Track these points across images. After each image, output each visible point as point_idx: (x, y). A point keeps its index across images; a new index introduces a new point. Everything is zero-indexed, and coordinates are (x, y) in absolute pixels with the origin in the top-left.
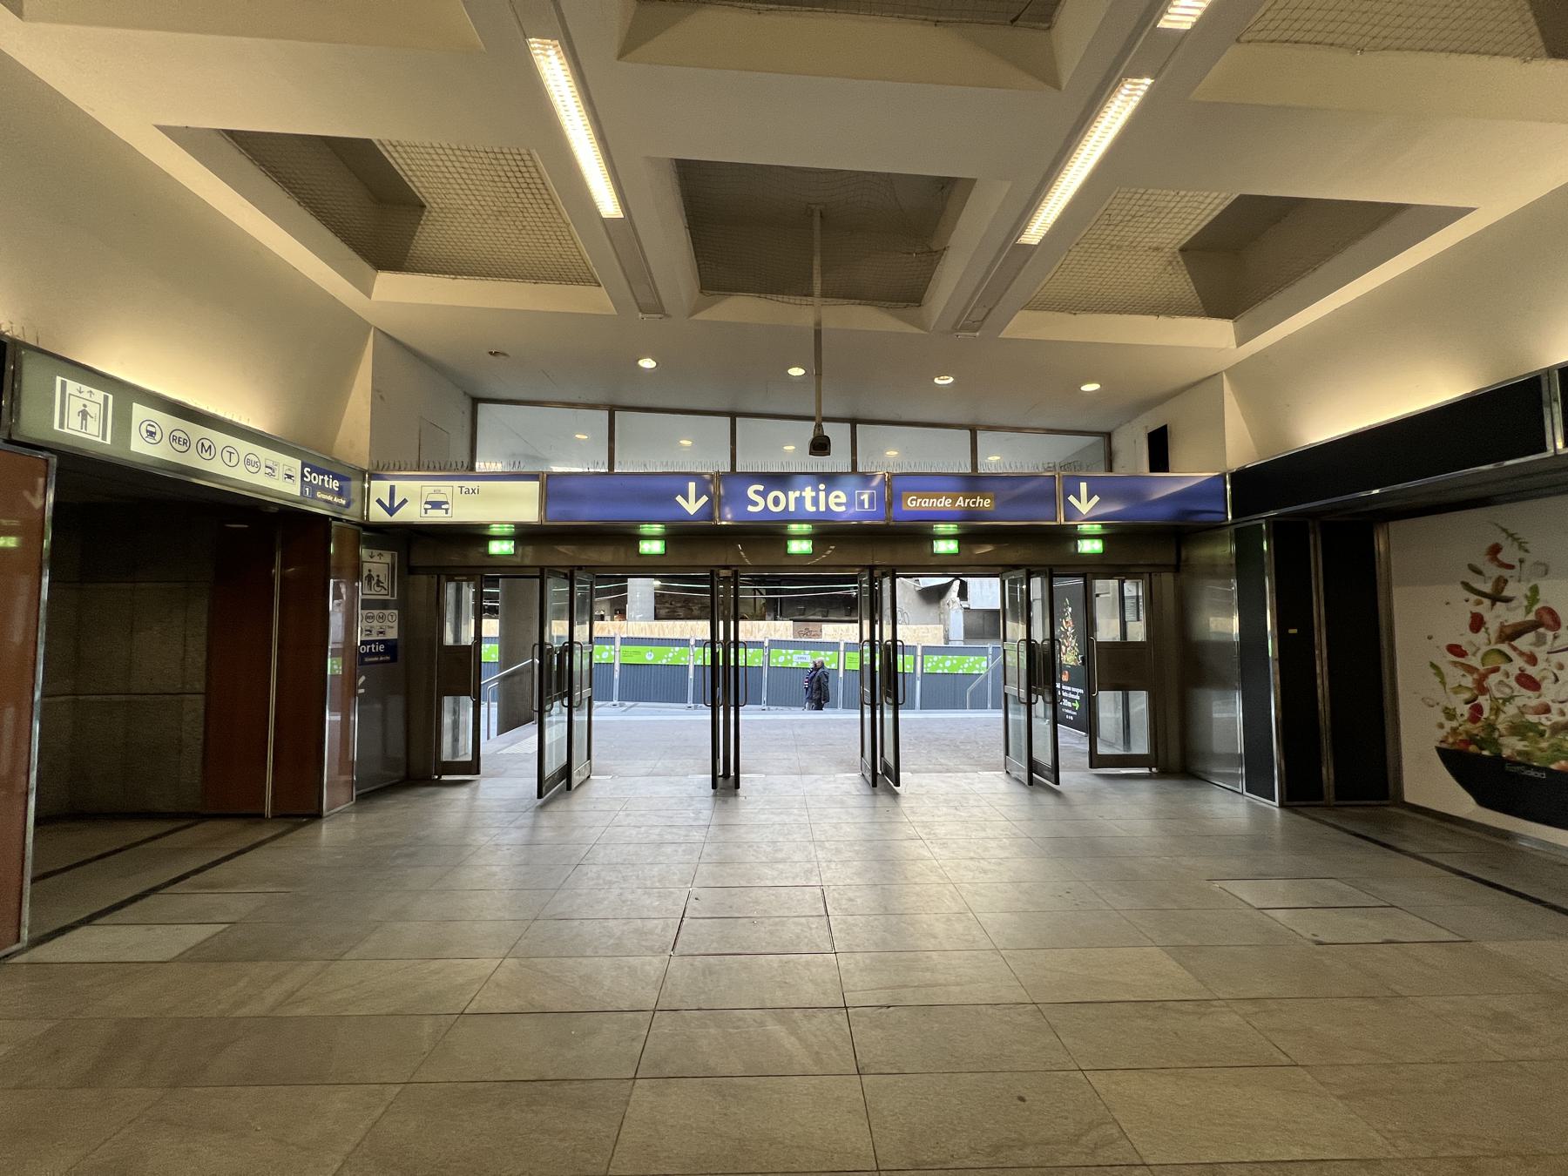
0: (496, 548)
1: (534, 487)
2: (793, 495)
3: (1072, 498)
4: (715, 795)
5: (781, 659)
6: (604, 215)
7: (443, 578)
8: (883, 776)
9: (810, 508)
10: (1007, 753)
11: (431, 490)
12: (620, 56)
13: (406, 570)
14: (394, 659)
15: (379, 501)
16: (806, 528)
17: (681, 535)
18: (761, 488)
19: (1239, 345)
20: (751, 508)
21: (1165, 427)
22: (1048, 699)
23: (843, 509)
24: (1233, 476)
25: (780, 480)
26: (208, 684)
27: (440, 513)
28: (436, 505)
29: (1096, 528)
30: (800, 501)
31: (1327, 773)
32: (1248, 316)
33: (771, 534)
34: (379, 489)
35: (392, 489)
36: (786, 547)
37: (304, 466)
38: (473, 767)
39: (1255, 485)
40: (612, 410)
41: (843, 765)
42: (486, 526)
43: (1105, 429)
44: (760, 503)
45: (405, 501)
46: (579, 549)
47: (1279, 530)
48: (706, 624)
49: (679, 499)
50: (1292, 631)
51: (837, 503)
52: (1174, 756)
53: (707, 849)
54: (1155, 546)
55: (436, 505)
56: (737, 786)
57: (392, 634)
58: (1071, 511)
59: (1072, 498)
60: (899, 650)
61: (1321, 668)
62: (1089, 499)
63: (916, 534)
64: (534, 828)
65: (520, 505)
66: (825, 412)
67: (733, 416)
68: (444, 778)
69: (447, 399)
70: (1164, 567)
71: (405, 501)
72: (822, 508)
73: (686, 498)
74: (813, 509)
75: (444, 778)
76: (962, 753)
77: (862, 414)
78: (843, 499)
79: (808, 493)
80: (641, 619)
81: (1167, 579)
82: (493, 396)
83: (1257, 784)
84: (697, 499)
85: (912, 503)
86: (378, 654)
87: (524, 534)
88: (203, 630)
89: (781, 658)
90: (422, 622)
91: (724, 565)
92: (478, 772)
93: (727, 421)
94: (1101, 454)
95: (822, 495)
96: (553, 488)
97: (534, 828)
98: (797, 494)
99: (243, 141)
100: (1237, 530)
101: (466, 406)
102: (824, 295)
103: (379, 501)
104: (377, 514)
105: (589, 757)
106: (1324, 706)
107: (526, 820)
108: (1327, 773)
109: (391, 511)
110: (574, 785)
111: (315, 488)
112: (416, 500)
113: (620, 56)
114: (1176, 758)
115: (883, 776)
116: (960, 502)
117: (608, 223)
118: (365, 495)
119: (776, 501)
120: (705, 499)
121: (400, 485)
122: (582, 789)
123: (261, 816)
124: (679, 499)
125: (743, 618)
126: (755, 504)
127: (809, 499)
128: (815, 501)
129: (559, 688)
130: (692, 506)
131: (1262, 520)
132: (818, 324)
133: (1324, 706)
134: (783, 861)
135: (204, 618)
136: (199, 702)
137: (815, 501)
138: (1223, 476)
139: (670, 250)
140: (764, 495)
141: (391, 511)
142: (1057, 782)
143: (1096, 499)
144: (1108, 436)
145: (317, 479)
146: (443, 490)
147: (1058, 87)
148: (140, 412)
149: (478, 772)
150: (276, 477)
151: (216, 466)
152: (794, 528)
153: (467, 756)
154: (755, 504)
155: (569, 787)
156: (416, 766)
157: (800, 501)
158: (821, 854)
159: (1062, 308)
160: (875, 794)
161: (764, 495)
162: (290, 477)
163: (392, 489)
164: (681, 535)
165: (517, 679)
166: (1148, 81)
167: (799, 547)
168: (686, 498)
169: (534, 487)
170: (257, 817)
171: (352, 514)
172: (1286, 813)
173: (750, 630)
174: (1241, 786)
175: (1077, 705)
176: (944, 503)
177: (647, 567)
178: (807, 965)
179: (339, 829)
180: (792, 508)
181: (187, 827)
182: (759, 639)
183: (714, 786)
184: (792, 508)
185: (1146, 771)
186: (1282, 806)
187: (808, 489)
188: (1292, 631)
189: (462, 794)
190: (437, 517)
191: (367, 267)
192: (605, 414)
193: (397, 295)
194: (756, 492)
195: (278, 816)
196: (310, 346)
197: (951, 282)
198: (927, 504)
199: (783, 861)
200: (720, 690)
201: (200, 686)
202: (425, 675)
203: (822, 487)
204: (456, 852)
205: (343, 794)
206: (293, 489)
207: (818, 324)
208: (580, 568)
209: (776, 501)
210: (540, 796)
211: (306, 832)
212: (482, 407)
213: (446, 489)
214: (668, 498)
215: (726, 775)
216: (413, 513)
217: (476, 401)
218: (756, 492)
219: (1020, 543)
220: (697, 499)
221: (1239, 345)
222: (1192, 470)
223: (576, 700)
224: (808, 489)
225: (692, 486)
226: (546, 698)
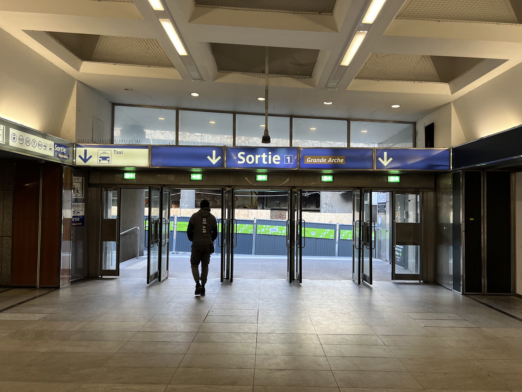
0: (127, 176)
1: (146, 151)
2: (257, 157)
3: (380, 159)
4: (222, 285)
5: (263, 230)
6: (180, 54)
7: (103, 189)
8: (295, 278)
9: (265, 162)
10: (353, 272)
11: (102, 152)
12: (189, 22)
13: (87, 186)
14: (83, 225)
15: (80, 156)
16: (264, 171)
17: (209, 172)
18: (244, 153)
19: (452, 93)
20: (239, 162)
21: (433, 123)
22: (368, 247)
23: (279, 163)
24: (453, 149)
25: (251, 150)
26: (13, 233)
27: (106, 162)
28: (104, 158)
29: (397, 172)
30: (260, 159)
31: (484, 281)
32: (457, 80)
33: (250, 172)
34: (80, 151)
35: (86, 151)
36: (256, 178)
37: (55, 144)
38: (116, 273)
39: (461, 154)
40: (178, 110)
41: (281, 276)
42: (123, 167)
43: (413, 121)
44: (242, 160)
45: (91, 157)
46: (164, 176)
47: (468, 175)
48: (220, 210)
49: (209, 157)
50: (471, 219)
51: (276, 160)
52: (431, 276)
53: (217, 300)
54: (420, 180)
55: (104, 158)
56: (232, 281)
57: (82, 214)
58: (380, 165)
59: (380, 159)
60: (303, 225)
61: (484, 237)
62: (388, 159)
63: (315, 173)
64: (147, 293)
65: (141, 159)
66: (270, 112)
67: (234, 113)
68: (103, 277)
69: (103, 108)
70: (429, 189)
71: (91, 157)
72: (270, 162)
73: (212, 158)
74: (266, 163)
75: (103, 277)
76: (336, 273)
77: (296, 113)
78: (279, 159)
79: (264, 156)
80: (188, 207)
81: (431, 195)
82: (122, 103)
83: (456, 287)
84: (216, 158)
85: (309, 161)
86: (77, 222)
87: (139, 171)
88: (11, 211)
89: (263, 230)
90: (94, 207)
91: (227, 183)
92: (118, 275)
93: (231, 115)
94: (411, 132)
95: (270, 157)
96: (155, 151)
97: (147, 293)
98: (259, 156)
99: (54, 35)
100: (454, 174)
101: (110, 107)
102: (270, 73)
103: (80, 156)
104: (79, 162)
105: (167, 269)
106: (484, 254)
107: (144, 290)
108: (484, 281)
109: (85, 160)
110: (162, 280)
111: (59, 152)
112: (95, 156)
113: (189, 22)
114: (429, 276)
115: (295, 278)
116: (330, 160)
117: (182, 57)
118: (74, 154)
119: (250, 159)
120: (219, 158)
121: (89, 150)
122: (165, 282)
123: (35, 287)
124: (209, 157)
125: (239, 207)
126: (241, 160)
127: (264, 158)
128: (267, 159)
129: (156, 238)
130: (214, 161)
131: (460, 170)
132: (267, 86)
133: (484, 254)
134: (247, 303)
135: (11, 205)
136: (10, 240)
137: (267, 159)
138: (449, 150)
139: (207, 63)
140: (245, 156)
141: (85, 160)
142: (371, 284)
143: (391, 159)
144: (415, 124)
145: (59, 149)
146: (107, 152)
147: (338, 32)
148: (12, 131)
149: (118, 275)
150: (44, 149)
151: (30, 148)
152: (260, 171)
153: (114, 268)
154: (241, 160)
155: (160, 280)
156: (91, 270)
157: (260, 159)
158: (261, 302)
159: (372, 79)
160: (291, 286)
161: (245, 156)
162: (51, 149)
163: (86, 151)
164: (209, 172)
165: (128, 236)
166: (366, 32)
167: (262, 178)
168: (212, 158)
169: (146, 151)
170: (34, 288)
171: (69, 162)
172: (465, 297)
173: (240, 214)
174: (451, 288)
175: (401, 254)
176: (323, 161)
177: (193, 185)
178: (247, 325)
179: (65, 292)
180: (257, 162)
181: (5, 291)
182: (252, 219)
183: (222, 281)
184: (257, 162)
185: (418, 282)
186: (463, 294)
187: (264, 154)
188: (471, 219)
189: (113, 282)
190: (104, 163)
191: (79, 60)
192: (174, 112)
193: (89, 69)
194: (242, 155)
195: (42, 288)
196: (52, 91)
197: (320, 72)
198: (315, 161)
199: (247, 303)
200: (225, 241)
201: (10, 234)
202: (95, 231)
203: (270, 153)
204: (118, 298)
205: (67, 281)
206: (51, 154)
207: (267, 86)
208: (164, 185)
209: (250, 159)
210: (148, 283)
211: (55, 293)
212: (117, 108)
213: (109, 151)
214: (204, 157)
215: (228, 278)
216: (94, 162)
217: (114, 105)
218: (242, 155)
219: (356, 177)
220: (216, 158)
221: (452, 93)
222: (441, 147)
223: (163, 243)
224: (264, 154)
225: (385, 154)
226: (151, 242)
